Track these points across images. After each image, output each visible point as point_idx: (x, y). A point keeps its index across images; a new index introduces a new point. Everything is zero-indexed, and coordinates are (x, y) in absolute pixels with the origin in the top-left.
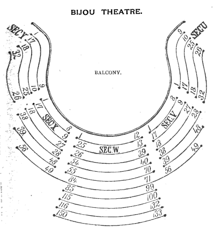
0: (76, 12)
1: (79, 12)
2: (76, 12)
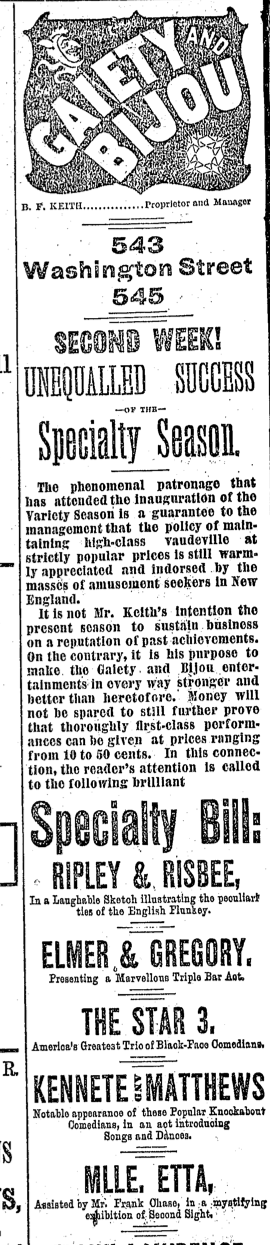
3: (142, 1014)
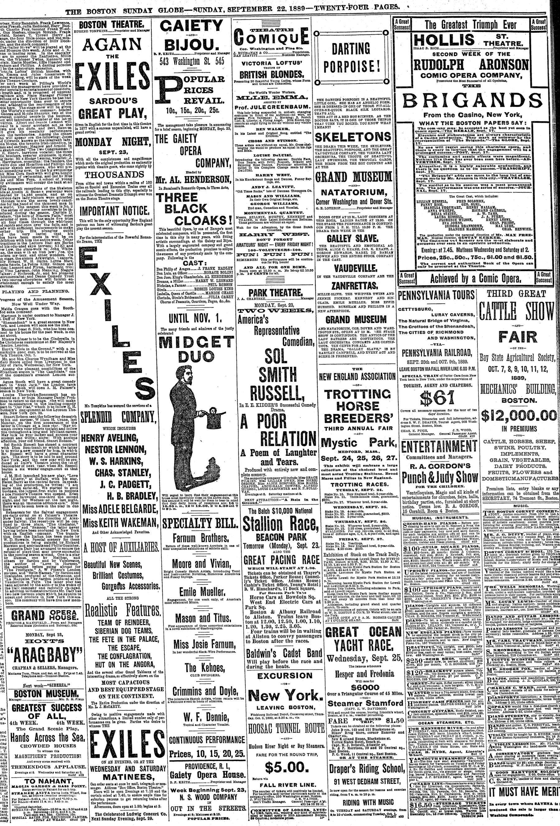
0: (175, 45)
1: (182, 44)
2: (175, 45)
3: (141, 82)
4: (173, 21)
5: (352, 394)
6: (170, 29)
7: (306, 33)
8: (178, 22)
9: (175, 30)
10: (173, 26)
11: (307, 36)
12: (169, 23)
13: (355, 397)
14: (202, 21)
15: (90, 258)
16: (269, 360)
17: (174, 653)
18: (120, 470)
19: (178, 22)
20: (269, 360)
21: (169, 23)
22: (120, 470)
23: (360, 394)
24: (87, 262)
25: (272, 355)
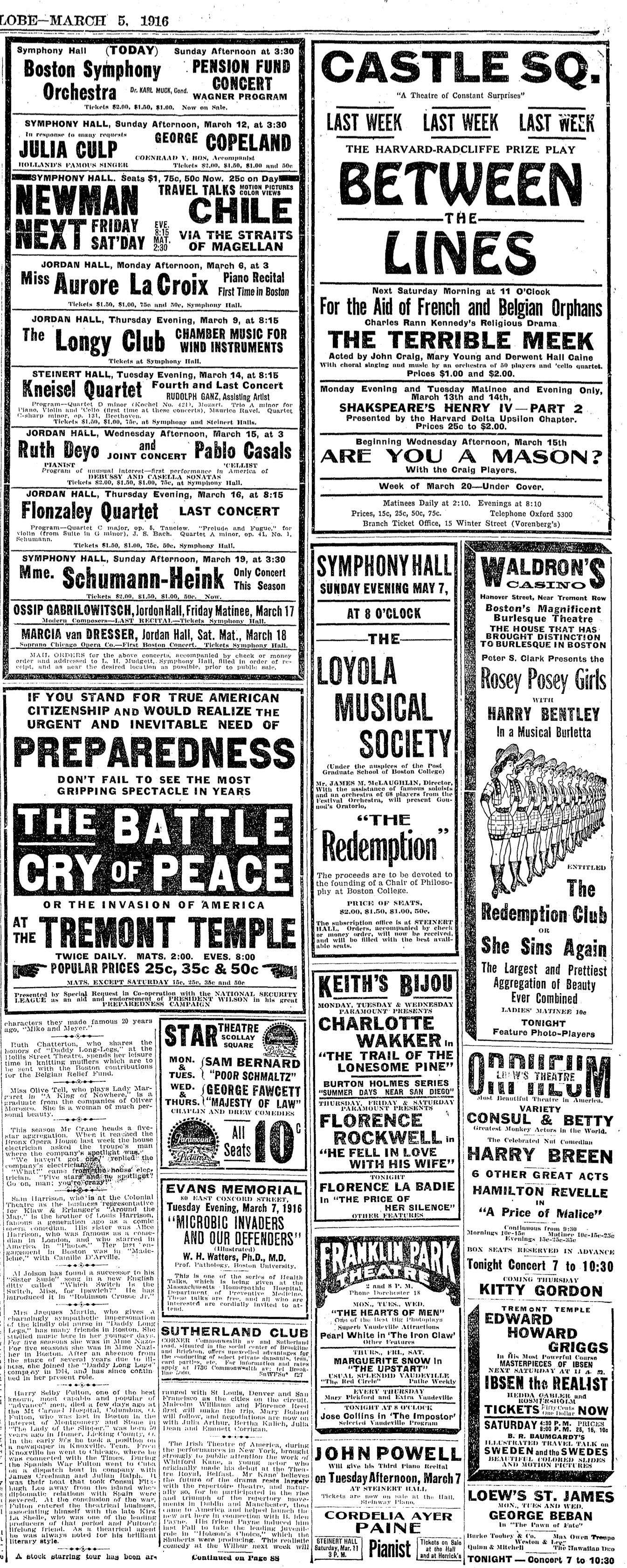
4: (358, 53)
5: (400, 1022)
6: (348, 74)
7: (290, 927)
8: (372, 57)
9: (360, 79)
10: (356, 66)
11: (292, 934)
12: (348, 59)
13: (405, 1028)
14: (426, 55)
15: (500, 66)
16: (367, 751)
17: (563, 64)
18: (137, 971)
19: (372, 57)
20: (367, 751)
21: (348, 59)
22: (137, 971)
23: (411, 1023)
24: (494, 72)
25: (372, 742)
